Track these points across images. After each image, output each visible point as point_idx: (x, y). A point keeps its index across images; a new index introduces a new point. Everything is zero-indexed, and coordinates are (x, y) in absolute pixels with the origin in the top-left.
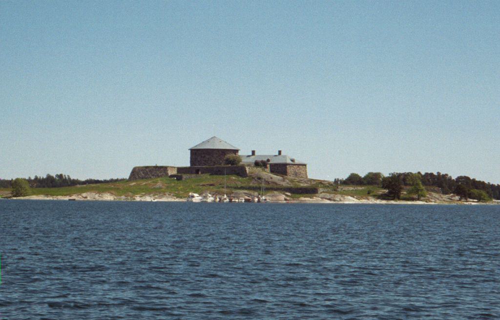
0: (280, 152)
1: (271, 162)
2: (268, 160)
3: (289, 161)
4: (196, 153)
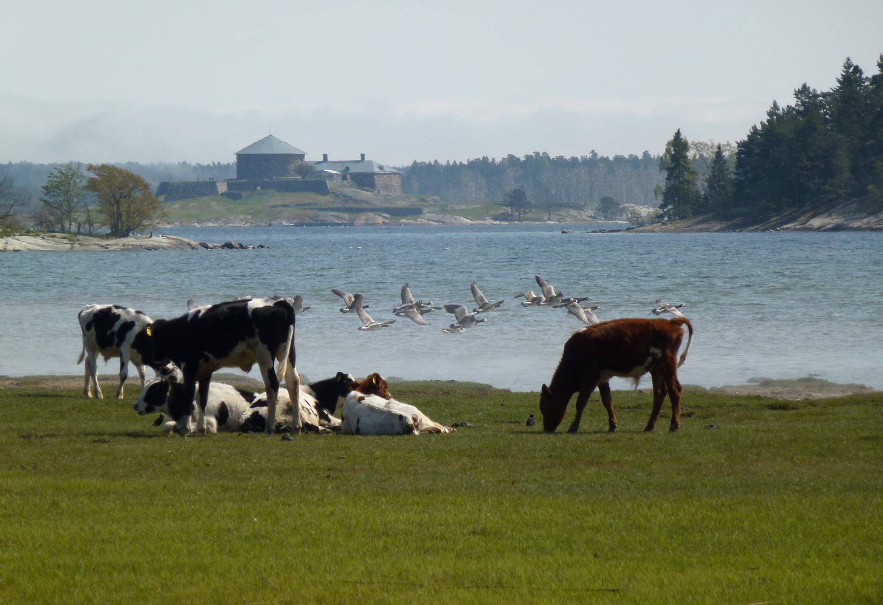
0: (363, 156)
1: (350, 171)
2: (347, 169)
3: (376, 170)
4: (240, 156)
